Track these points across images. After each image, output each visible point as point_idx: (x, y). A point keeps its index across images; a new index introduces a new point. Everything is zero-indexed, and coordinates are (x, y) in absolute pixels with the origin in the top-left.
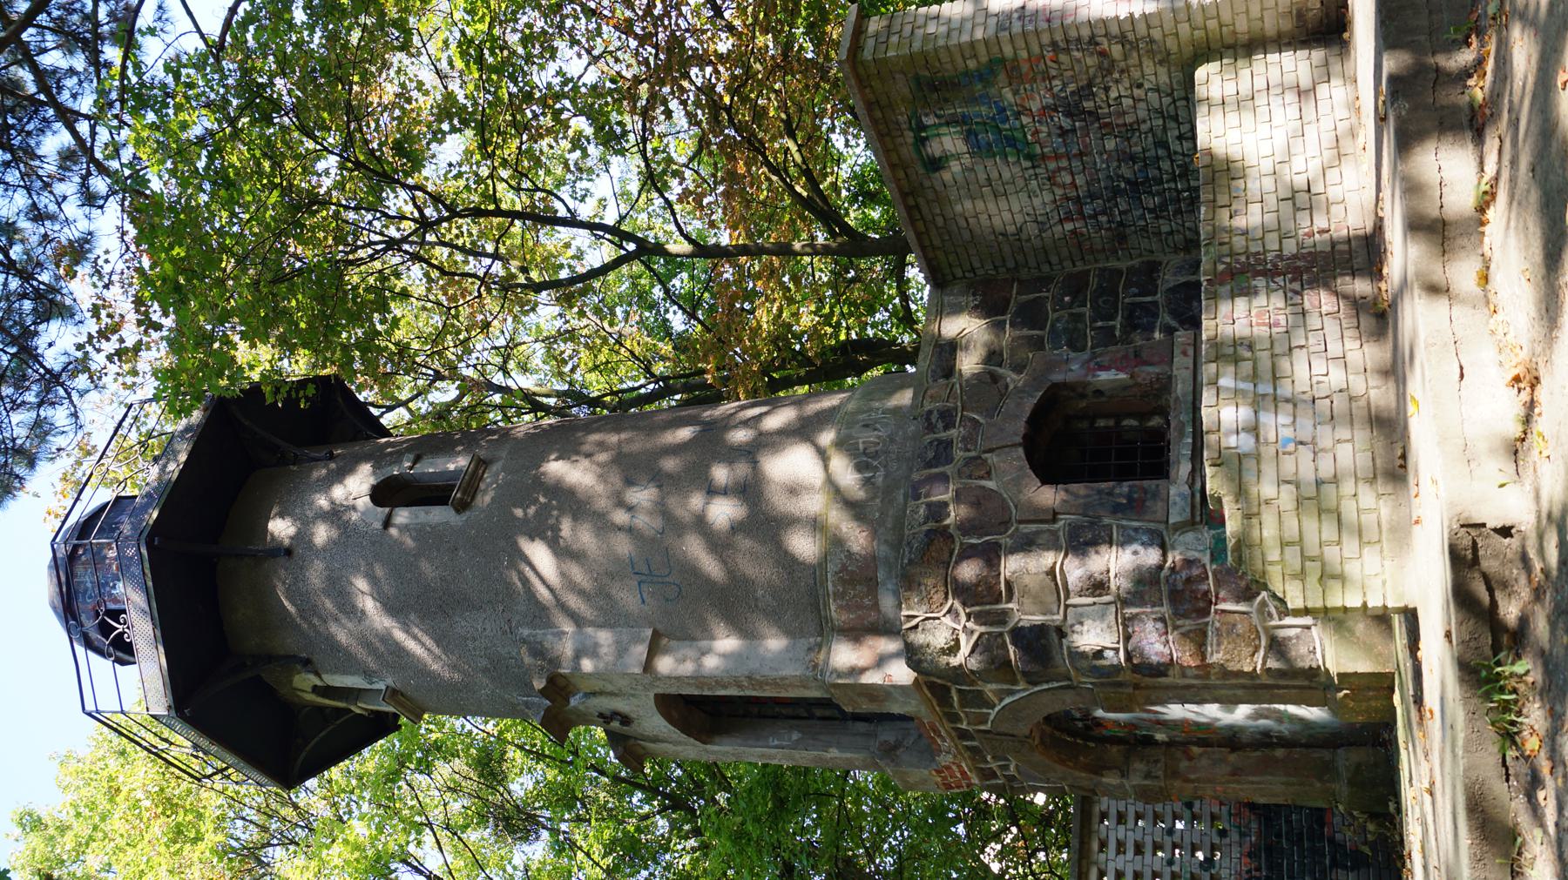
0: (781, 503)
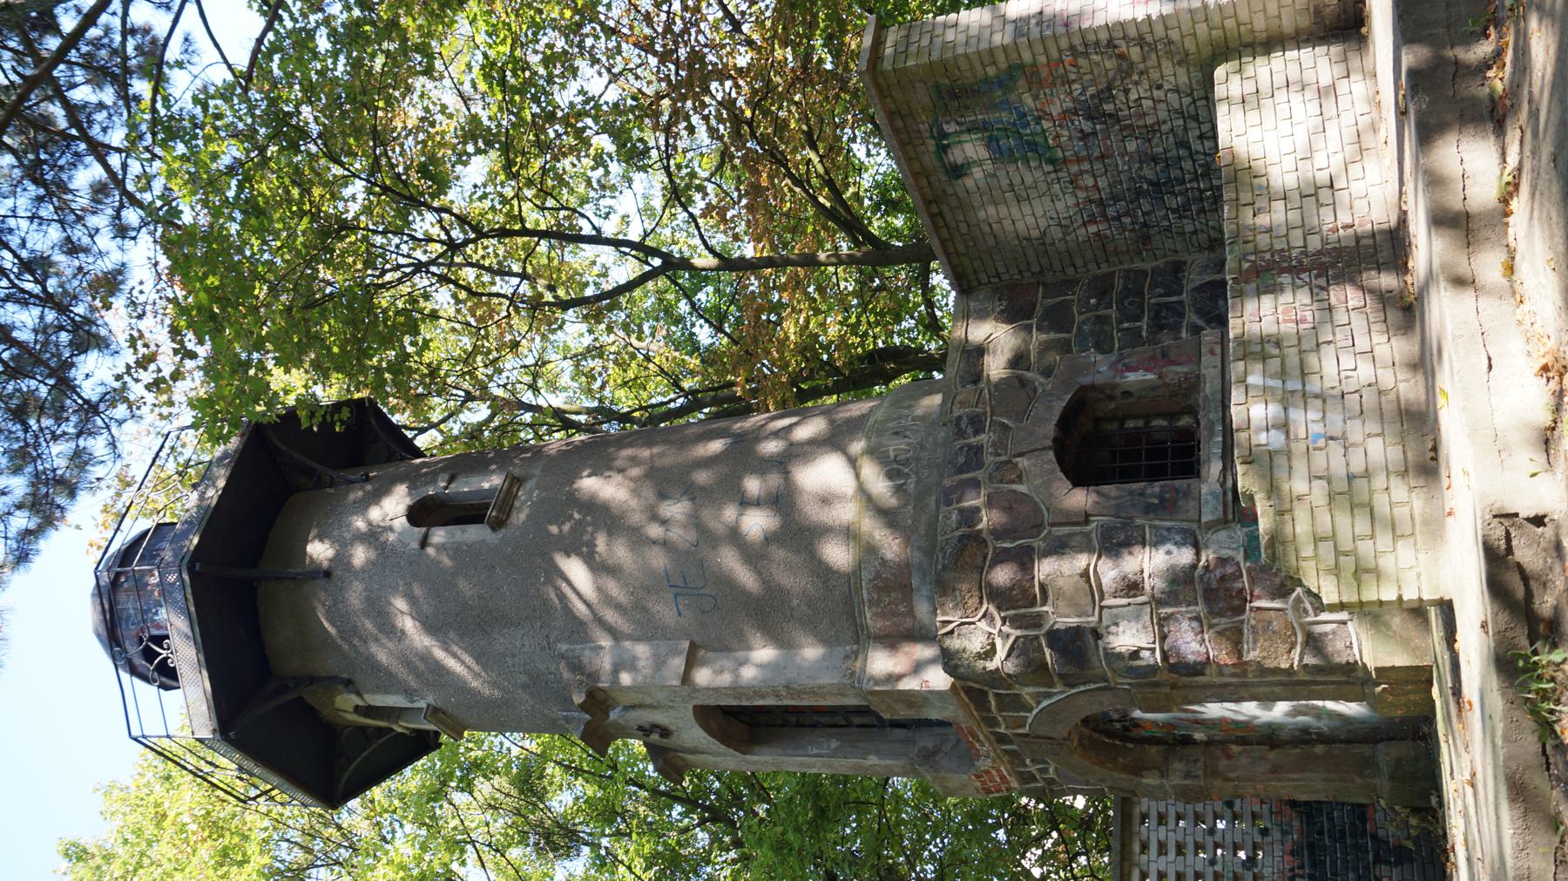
0: (814, 513)
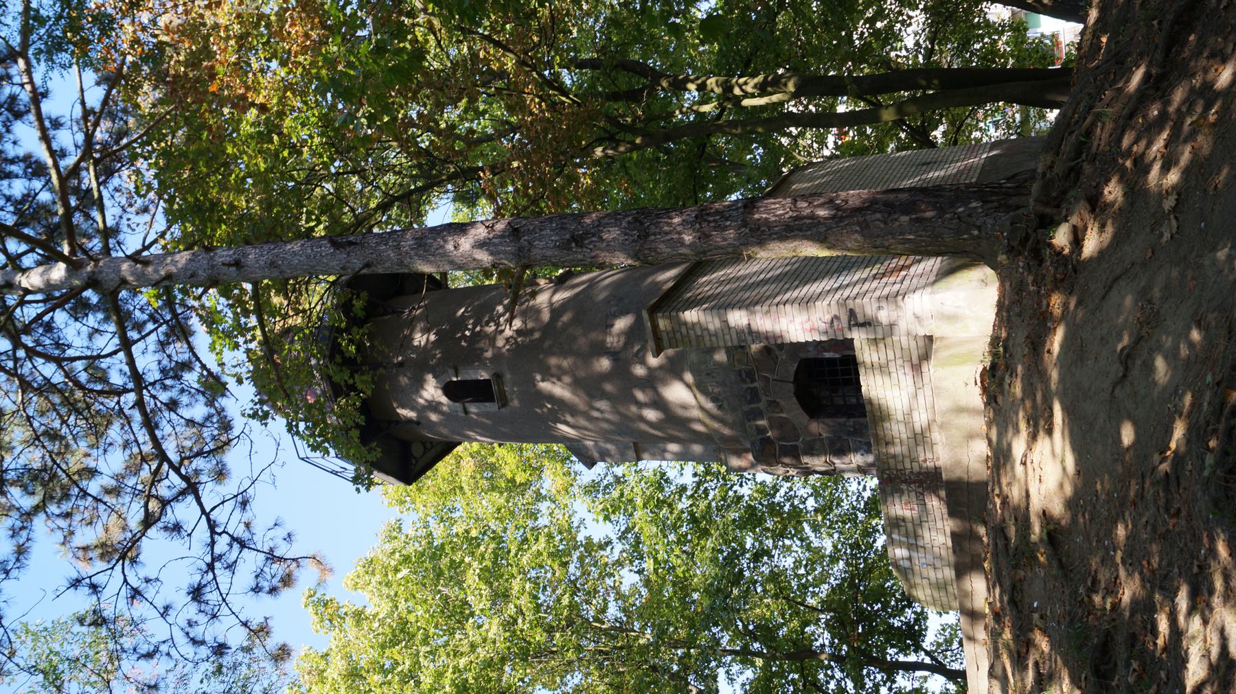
0: (681, 412)
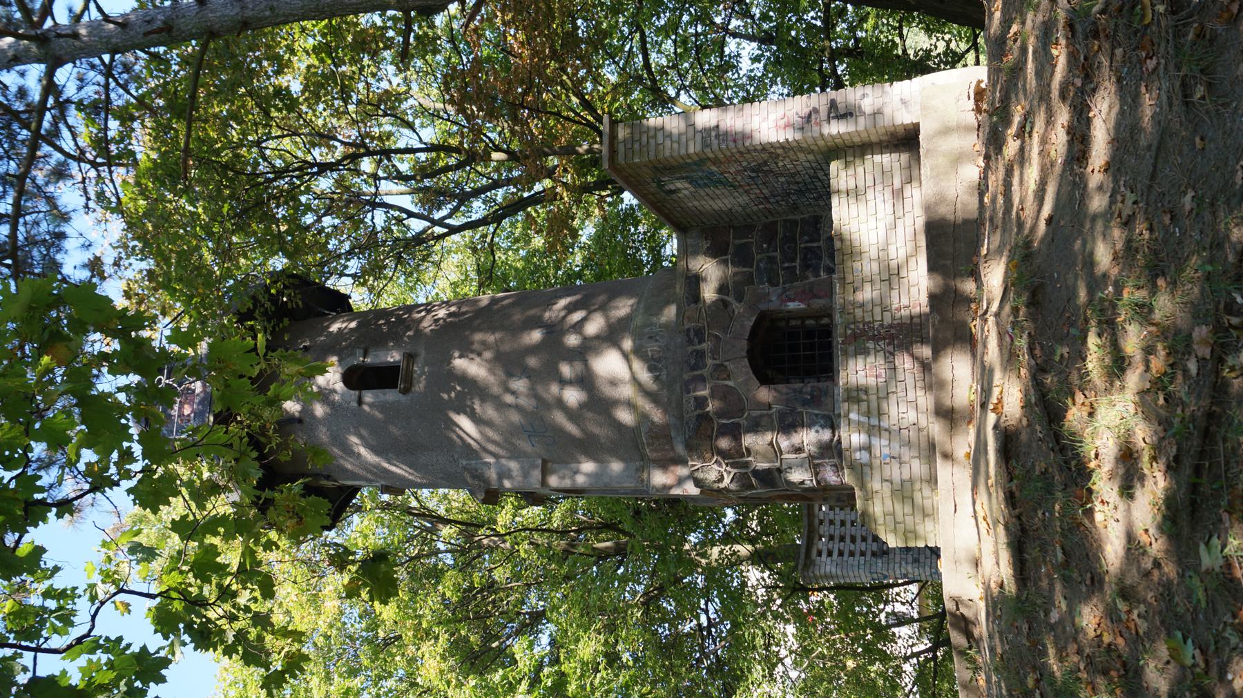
0: (608, 391)
